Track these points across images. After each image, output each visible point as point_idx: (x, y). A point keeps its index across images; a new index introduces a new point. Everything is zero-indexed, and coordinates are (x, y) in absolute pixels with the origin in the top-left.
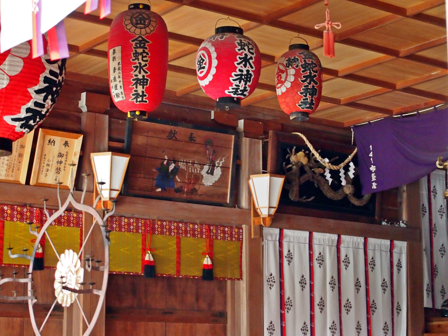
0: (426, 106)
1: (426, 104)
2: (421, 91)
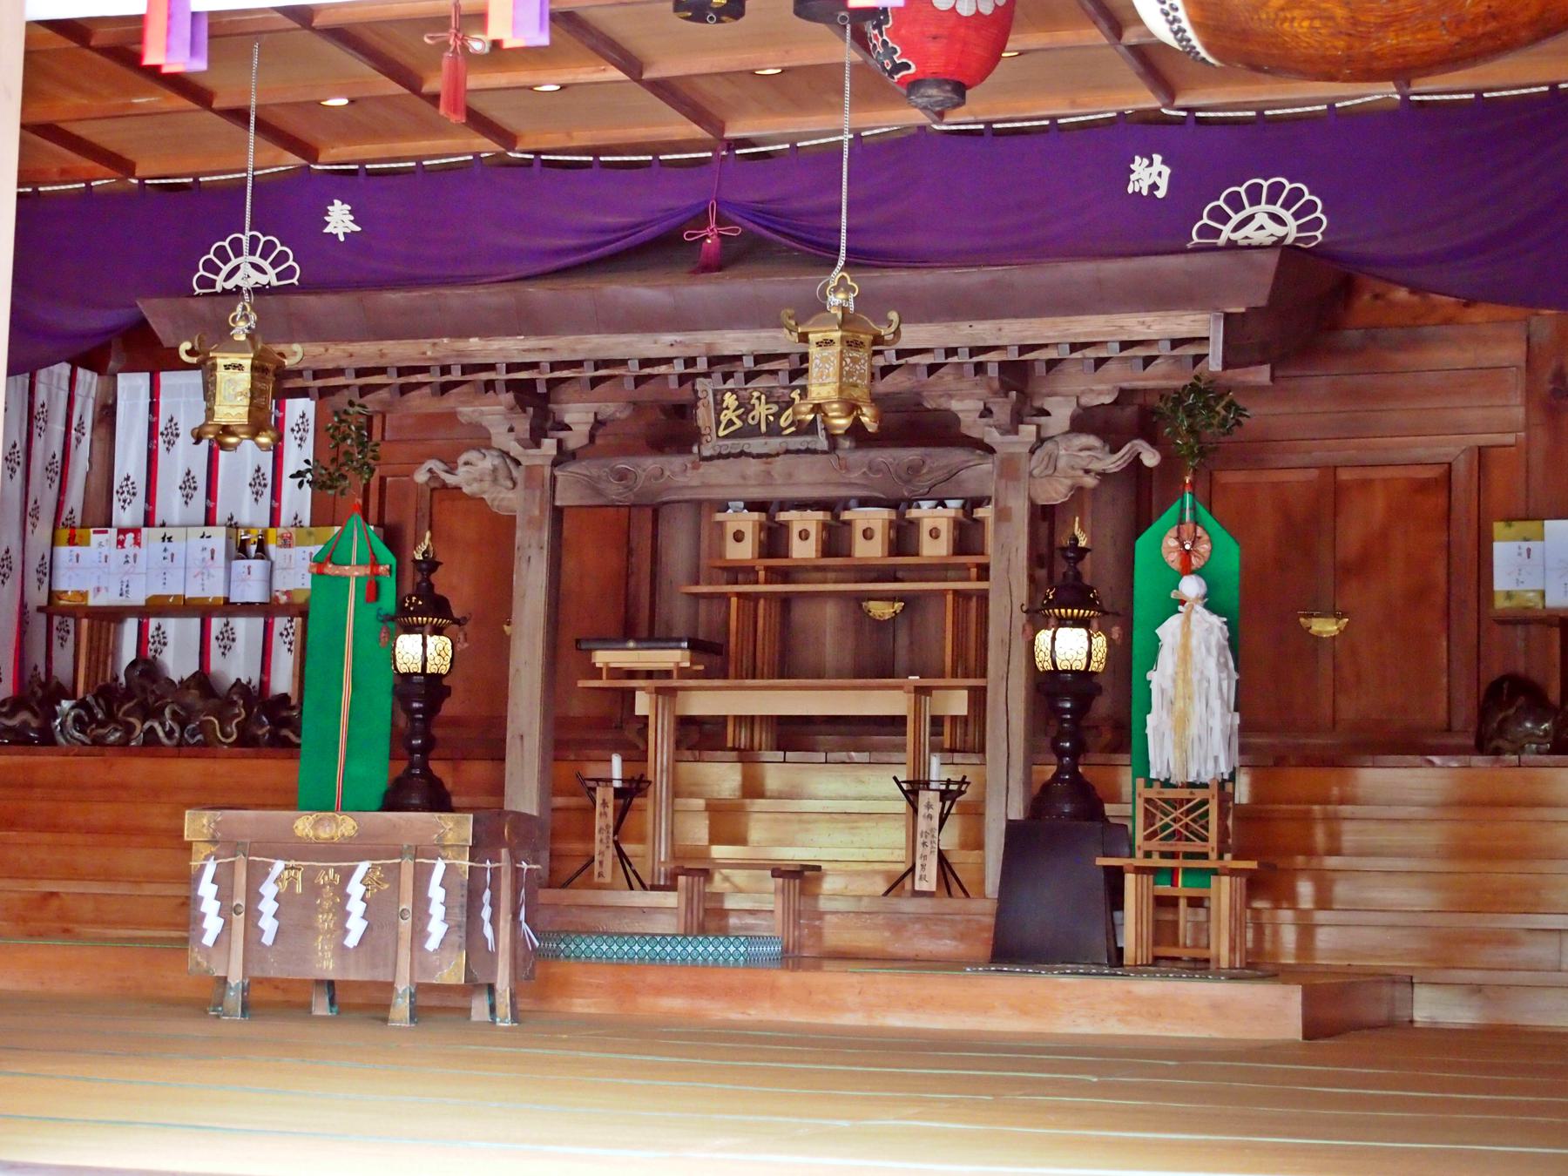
0: (63, 178)
1: (63, 172)
2: (79, 138)
